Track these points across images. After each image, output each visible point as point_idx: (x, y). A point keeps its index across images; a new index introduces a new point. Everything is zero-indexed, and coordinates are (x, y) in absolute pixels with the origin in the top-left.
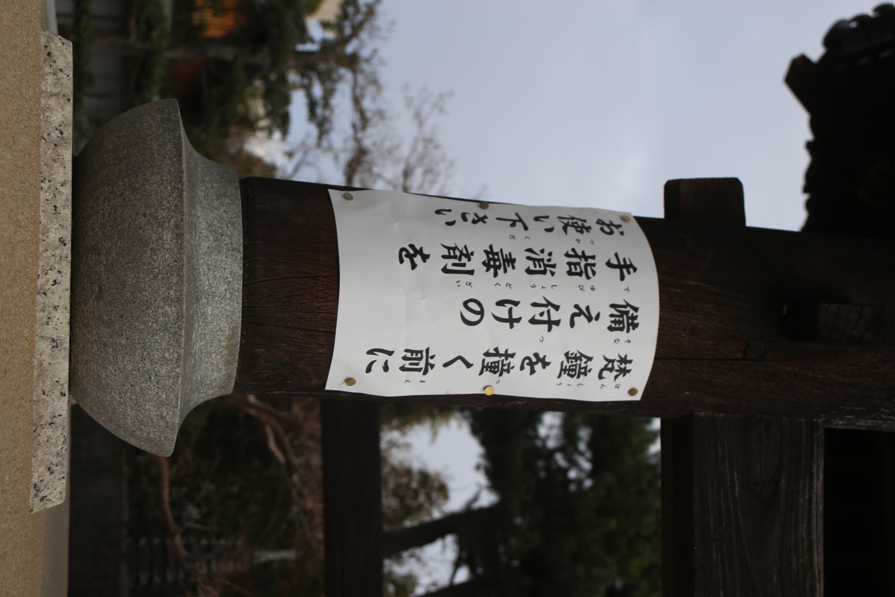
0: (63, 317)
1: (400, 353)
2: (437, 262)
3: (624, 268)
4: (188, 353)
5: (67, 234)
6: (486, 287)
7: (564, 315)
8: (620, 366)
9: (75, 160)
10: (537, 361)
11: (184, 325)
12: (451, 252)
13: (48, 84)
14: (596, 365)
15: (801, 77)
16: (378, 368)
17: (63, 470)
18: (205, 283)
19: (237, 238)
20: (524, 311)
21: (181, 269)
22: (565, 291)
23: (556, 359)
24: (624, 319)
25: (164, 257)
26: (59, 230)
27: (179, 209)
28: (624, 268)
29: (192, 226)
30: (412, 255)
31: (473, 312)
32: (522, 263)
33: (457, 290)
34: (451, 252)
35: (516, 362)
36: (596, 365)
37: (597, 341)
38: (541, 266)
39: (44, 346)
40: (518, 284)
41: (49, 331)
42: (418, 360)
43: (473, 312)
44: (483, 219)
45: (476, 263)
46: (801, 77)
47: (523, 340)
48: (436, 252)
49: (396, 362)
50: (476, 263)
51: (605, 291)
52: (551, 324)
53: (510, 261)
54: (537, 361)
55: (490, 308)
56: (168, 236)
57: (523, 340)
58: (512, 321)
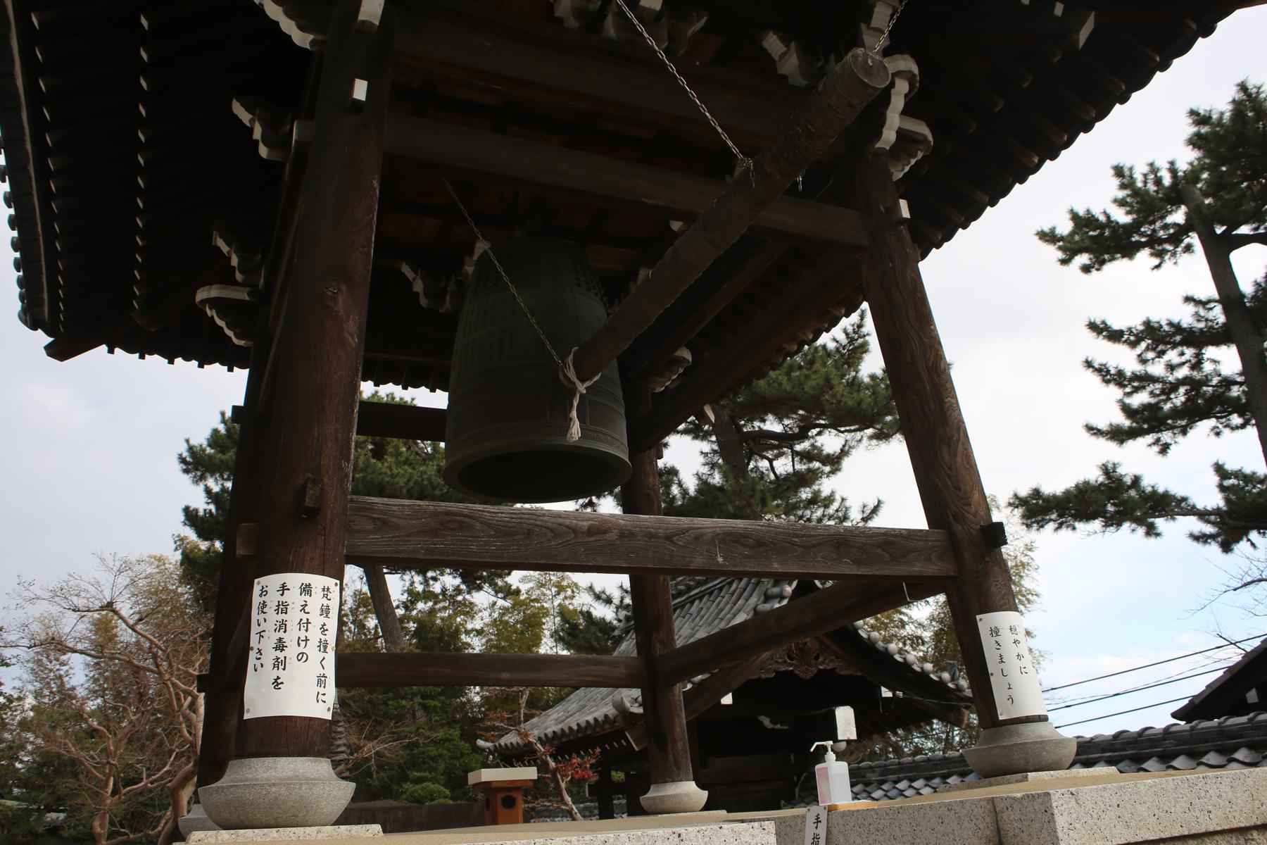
0: (308, 830)
1: (318, 689)
2: (280, 673)
3: (284, 588)
4: (319, 779)
5: (274, 830)
6: (292, 651)
7: (304, 617)
8: (326, 590)
9: (226, 827)
10: (323, 629)
11: (309, 781)
12: (276, 666)
13: (212, 840)
14: (325, 602)
15: (61, 350)
16: (324, 698)
17: (368, 826)
18: (290, 773)
19: (270, 759)
20: (303, 634)
21: (287, 783)
22: (294, 616)
23: (323, 620)
24: (306, 589)
25: (283, 791)
26: (273, 833)
27: (262, 785)
28: (284, 588)
29: (267, 779)
30: (277, 683)
31: (302, 657)
32: (281, 634)
33: (292, 663)
34: (276, 666)
35: (323, 638)
36: (325, 602)
37: (316, 601)
38: (283, 626)
39: (320, 836)
40: (290, 637)
41: (314, 834)
42: (321, 681)
43: (302, 657)
44: (260, 651)
45: (281, 655)
46: (61, 350)
47: (314, 634)
48: (276, 673)
49: (322, 690)
50: (281, 655)
51: (294, 598)
52: (308, 623)
53: (280, 639)
54: (323, 629)
55: (301, 649)
56: (274, 789)
57: (314, 634)
58: (307, 640)
